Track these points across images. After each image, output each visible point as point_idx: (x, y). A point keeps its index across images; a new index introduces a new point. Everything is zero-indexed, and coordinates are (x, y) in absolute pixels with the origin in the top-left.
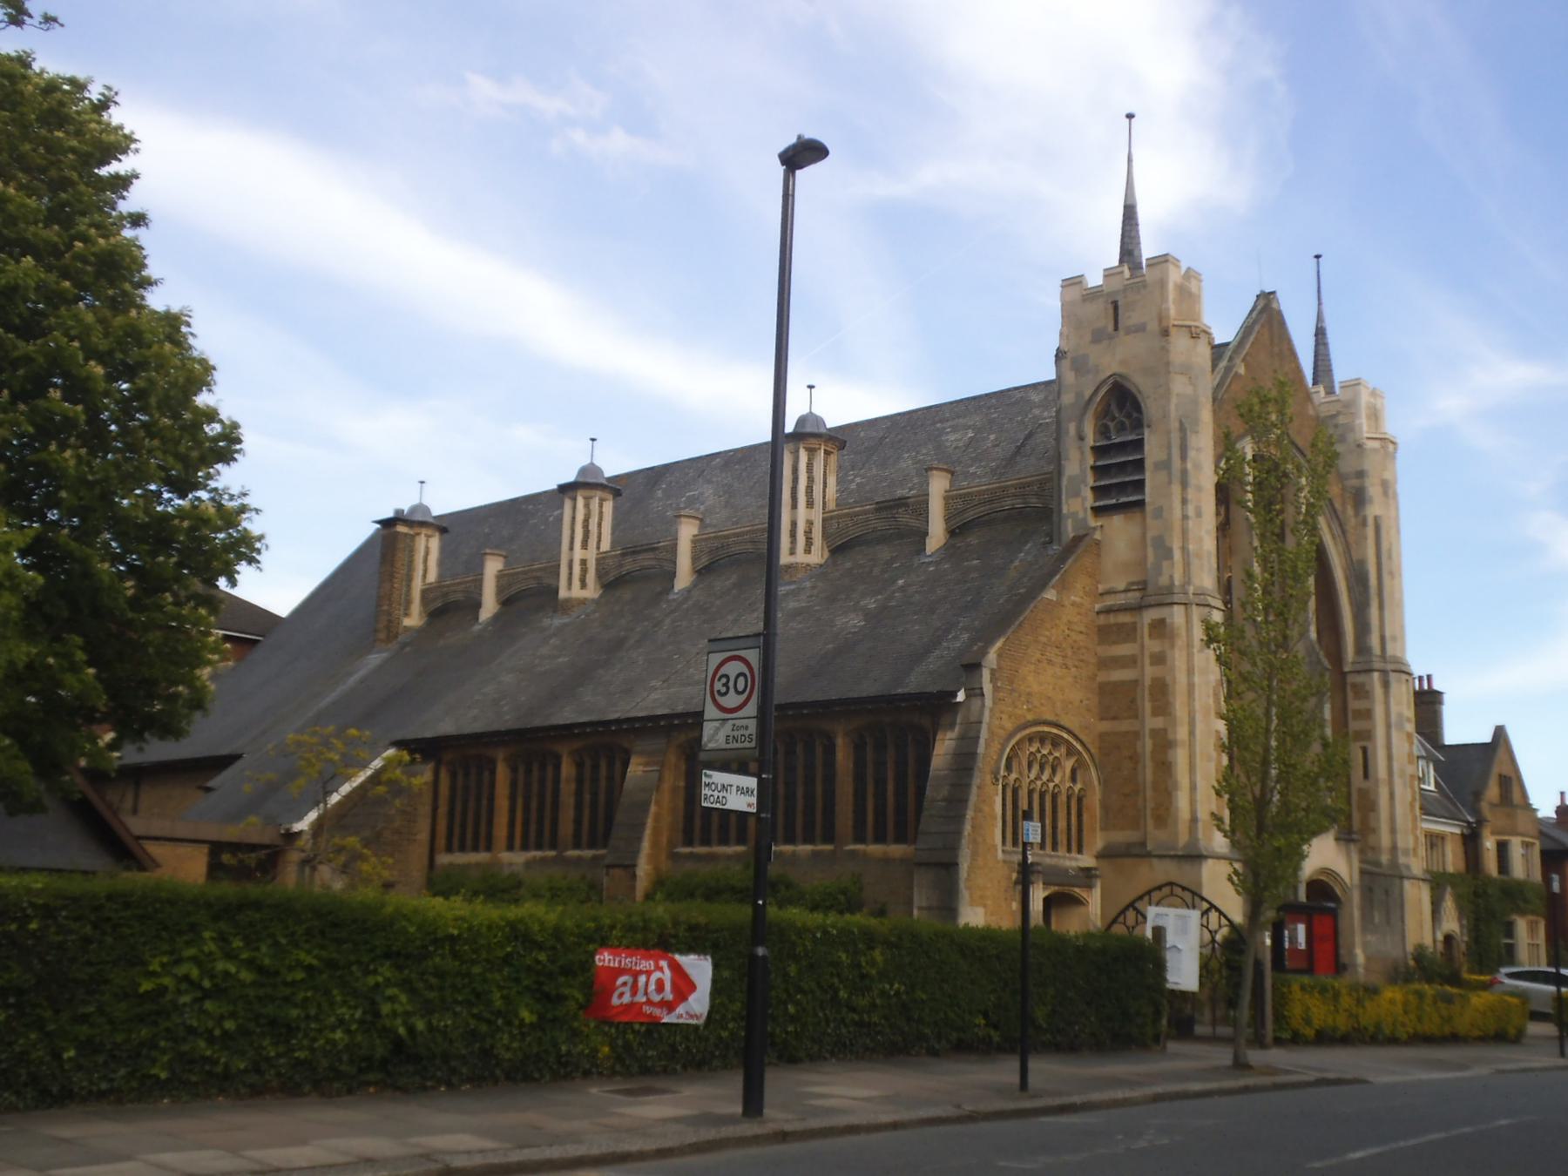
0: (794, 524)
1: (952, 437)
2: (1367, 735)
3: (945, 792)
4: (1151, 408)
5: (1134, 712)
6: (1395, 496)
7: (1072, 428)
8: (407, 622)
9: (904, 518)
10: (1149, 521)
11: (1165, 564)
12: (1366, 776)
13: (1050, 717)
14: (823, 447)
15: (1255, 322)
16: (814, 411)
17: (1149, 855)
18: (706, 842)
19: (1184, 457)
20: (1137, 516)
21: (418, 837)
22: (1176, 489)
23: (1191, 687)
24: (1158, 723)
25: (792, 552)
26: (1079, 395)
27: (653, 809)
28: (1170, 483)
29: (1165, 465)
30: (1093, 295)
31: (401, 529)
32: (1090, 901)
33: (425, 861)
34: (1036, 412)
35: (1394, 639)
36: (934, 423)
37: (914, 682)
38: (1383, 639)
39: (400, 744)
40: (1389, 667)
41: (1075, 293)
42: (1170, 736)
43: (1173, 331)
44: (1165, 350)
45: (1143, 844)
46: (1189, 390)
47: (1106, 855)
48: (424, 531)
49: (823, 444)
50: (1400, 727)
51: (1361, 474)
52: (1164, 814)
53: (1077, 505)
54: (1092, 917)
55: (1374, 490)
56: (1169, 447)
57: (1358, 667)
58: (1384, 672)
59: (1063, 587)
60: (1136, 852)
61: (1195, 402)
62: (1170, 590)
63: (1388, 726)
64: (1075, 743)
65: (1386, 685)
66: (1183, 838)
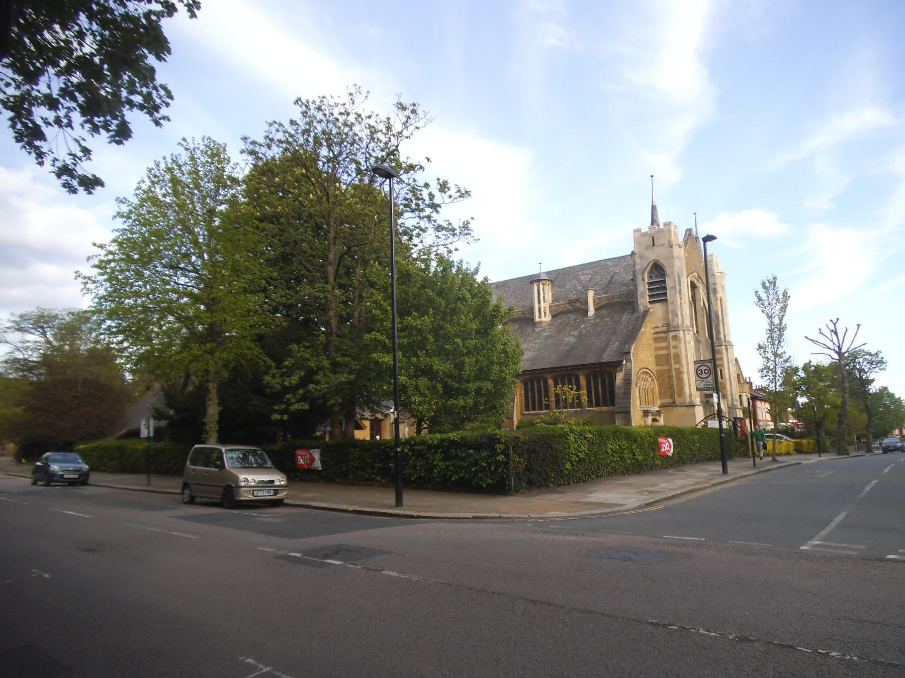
0: (540, 309)
1: (583, 277)
2: (722, 365)
3: (623, 390)
4: (668, 270)
5: (669, 364)
7: (640, 277)
9: (578, 305)
10: (669, 305)
11: (675, 318)
12: (722, 378)
13: (645, 367)
15: (688, 239)
17: (677, 406)
18: (534, 409)
19: (680, 285)
20: (665, 304)
22: (678, 295)
23: (687, 355)
24: (677, 366)
25: (540, 317)
26: (642, 266)
28: (676, 293)
29: (674, 288)
30: (645, 235)
34: (613, 268)
35: (728, 335)
36: (574, 273)
37: (605, 358)
38: (725, 335)
40: (727, 344)
41: (638, 234)
42: (681, 370)
43: (674, 246)
44: (672, 252)
45: (674, 403)
46: (680, 264)
47: (662, 406)
50: (732, 363)
51: (715, 284)
52: (681, 393)
53: (643, 301)
55: (719, 289)
56: (675, 283)
58: (726, 346)
59: (645, 327)
60: (673, 405)
61: (682, 267)
62: (678, 326)
63: (728, 362)
65: (727, 350)
66: (688, 400)
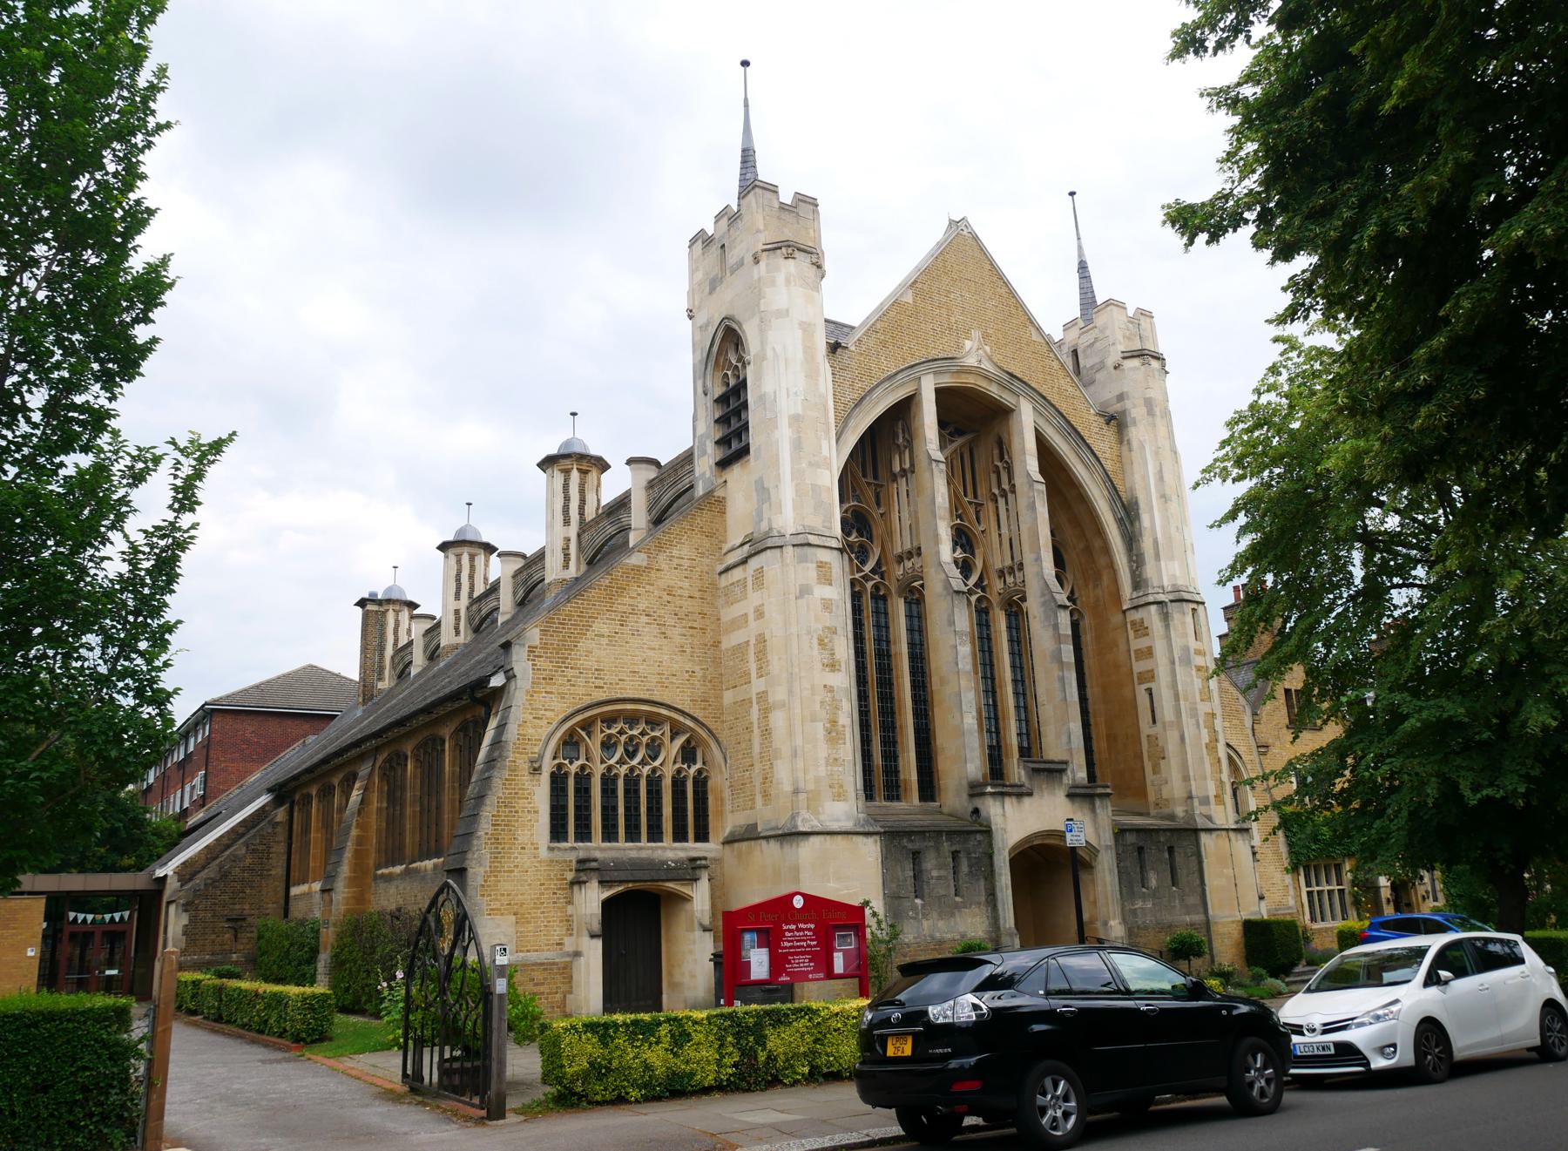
2: (1150, 676)
6: (1166, 414)
8: (380, 685)
14: (575, 467)
16: (577, 436)
21: (273, 872)
27: (354, 832)
31: (370, 607)
32: (694, 896)
33: (282, 893)
39: (270, 790)
48: (391, 607)
49: (575, 463)
54: (698, 915)
57: (1136, 603)
64: (681, 719)
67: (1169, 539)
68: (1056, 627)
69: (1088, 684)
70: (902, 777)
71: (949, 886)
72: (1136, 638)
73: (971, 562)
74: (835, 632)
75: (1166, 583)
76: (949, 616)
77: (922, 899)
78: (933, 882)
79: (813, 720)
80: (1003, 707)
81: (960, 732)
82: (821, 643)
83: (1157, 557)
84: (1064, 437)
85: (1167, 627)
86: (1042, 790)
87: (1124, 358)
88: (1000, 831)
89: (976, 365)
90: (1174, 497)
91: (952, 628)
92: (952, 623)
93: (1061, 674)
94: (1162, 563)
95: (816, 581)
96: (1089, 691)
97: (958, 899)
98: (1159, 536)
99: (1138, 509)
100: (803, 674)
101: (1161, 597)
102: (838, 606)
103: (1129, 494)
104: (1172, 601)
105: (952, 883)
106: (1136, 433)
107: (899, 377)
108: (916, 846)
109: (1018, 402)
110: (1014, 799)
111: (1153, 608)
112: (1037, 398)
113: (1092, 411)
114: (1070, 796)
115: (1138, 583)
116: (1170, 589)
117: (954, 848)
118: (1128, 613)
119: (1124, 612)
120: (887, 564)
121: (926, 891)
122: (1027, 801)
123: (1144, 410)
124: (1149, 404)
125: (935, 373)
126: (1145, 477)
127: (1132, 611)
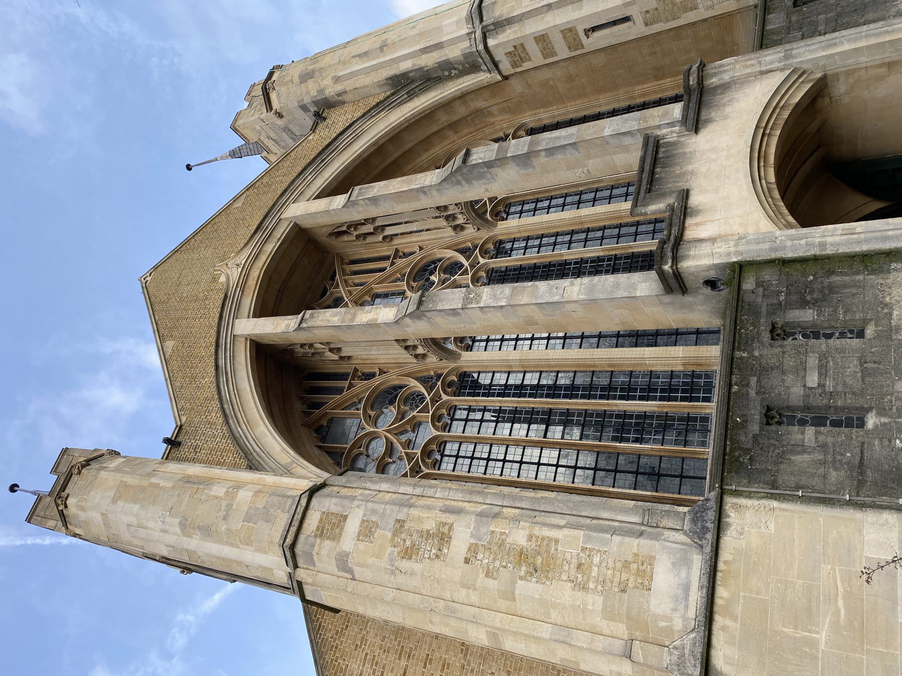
2: (569, 33)
57: (491, 65)
67: (421, 35)
68: (489, 165)
69: (597, 110)
70: (681, 368)
71: (841, 351)
72: (530, 60)
73: (448, 262)
74: (401, 522)
75: (465, 31)
76: (448, 315)
77: (869, 410)
78: (830, 384)
79: (509, 595)
80: (606, 219)
81: (591, 303)
82: (408, 553)
83: (439, 46)
84: (327, 165)
85: (509, 21)
86: (683, 174)
87: (271, 109)
88: (741, 248)
89: (240, 270)
90: (385, 37)
91: (460, 311)
92: (454, 312)
93: (543, 153)
94: (444, 39)
95: (334, 544)
96: (604, 109)
97: (870, 331)
98: (418, 47)
99: (397, 76)
100: (448, 596)
101: (479, 33)
102: (374, 512)
103: (386, 88)
104: (481, 20)
105: (834, 342)
106: (331, 90)
107: (221, 362)
108: (756, 414)
109: (286, 219)
110: (689, 221)
111: (491, 42)
112: (284, 199)
113: (311, 138)
114: (697, 131)
115: (470, 66)
116: (470, 26)
117: (766, 336)
118: (505, 73)
119: (506, 78)
120: (427, 370)
121: (850, 401)
122: (695, 200)
123: (310, 82)
124: (306, 77)
125: (236, 317)
126: (367, 71)
127: (501, 67)
